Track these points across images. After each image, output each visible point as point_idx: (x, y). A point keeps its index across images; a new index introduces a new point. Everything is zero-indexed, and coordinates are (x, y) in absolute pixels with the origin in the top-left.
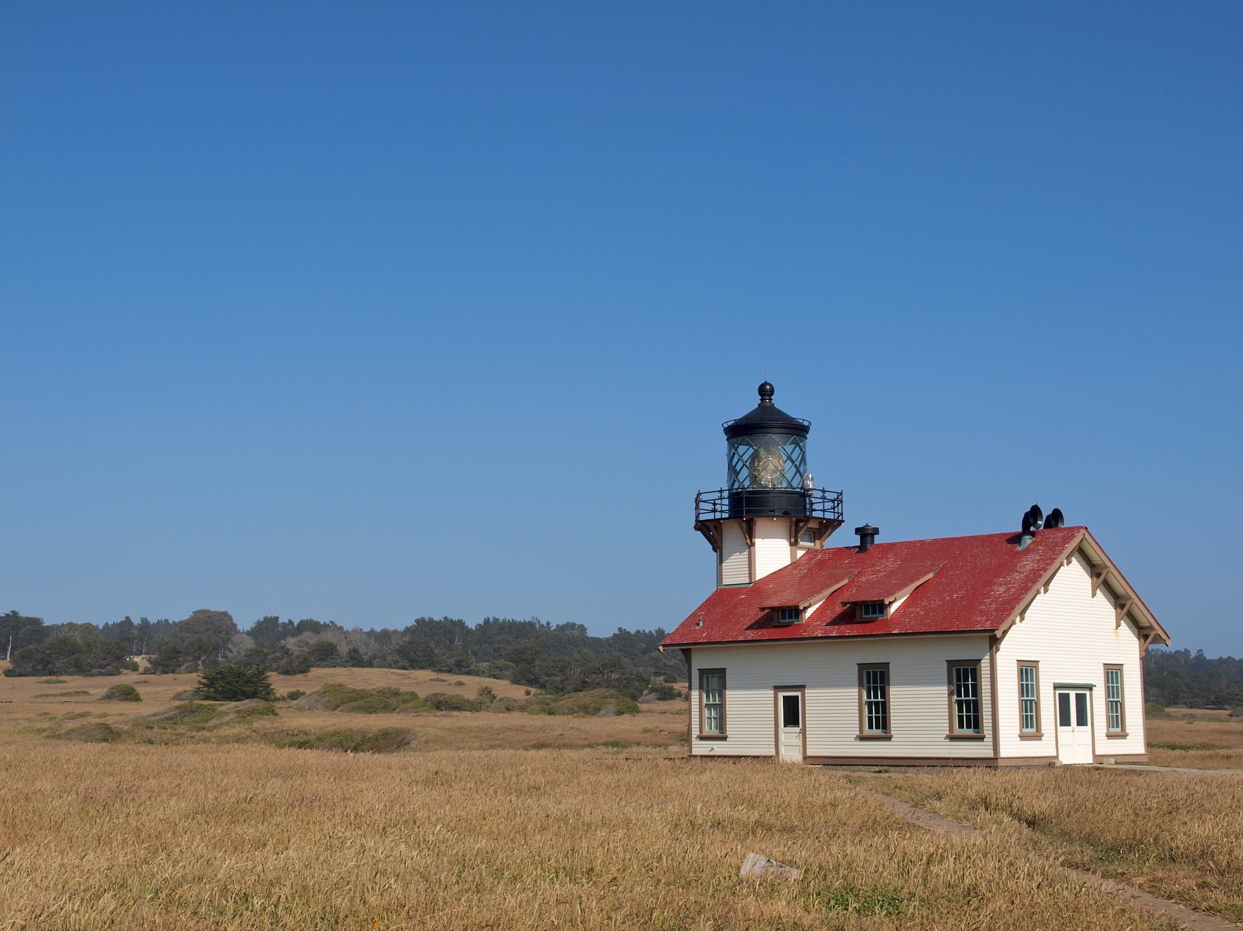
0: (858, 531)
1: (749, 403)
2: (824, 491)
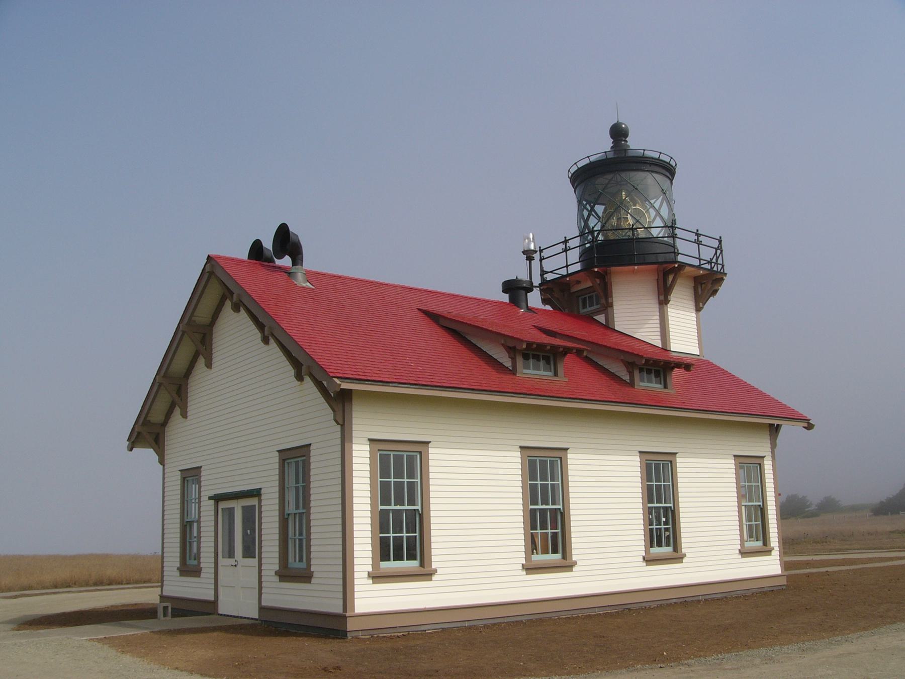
1: (603, 145)
2: (698, 234)
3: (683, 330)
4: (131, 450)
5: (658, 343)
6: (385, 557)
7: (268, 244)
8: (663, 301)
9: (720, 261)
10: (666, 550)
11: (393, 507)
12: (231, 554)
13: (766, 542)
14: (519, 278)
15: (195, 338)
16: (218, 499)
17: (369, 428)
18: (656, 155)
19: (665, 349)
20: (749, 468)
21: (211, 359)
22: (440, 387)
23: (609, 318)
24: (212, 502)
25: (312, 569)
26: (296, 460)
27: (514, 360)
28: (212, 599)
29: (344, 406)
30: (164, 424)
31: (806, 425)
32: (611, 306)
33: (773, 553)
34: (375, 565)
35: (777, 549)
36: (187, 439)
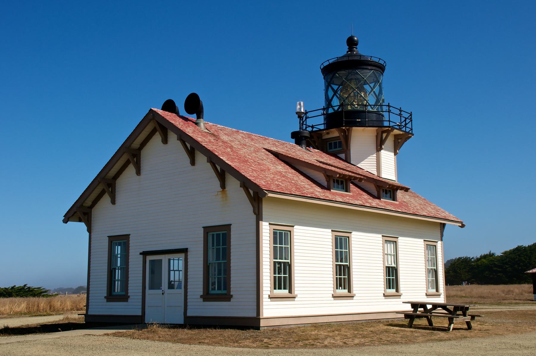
1: (342, 50)
2: (401, 111)
3: (386, 166)
4: (65, 221)
5: (375, 173)
8: (379, 148)
9: (409, 125)
10: (393, 291)
11: (284, 261)
13: (437, 290)
18: (377, 60)
20: (431, 248)
21: (140, 167)
22: (280, 192)
24: (142, 256)
25: (231, 294)
27: (328, 182)
28: (139, 313)
31: (460, 225)
33: (441, 296)
35: (443, 294)
36: (111, 217)
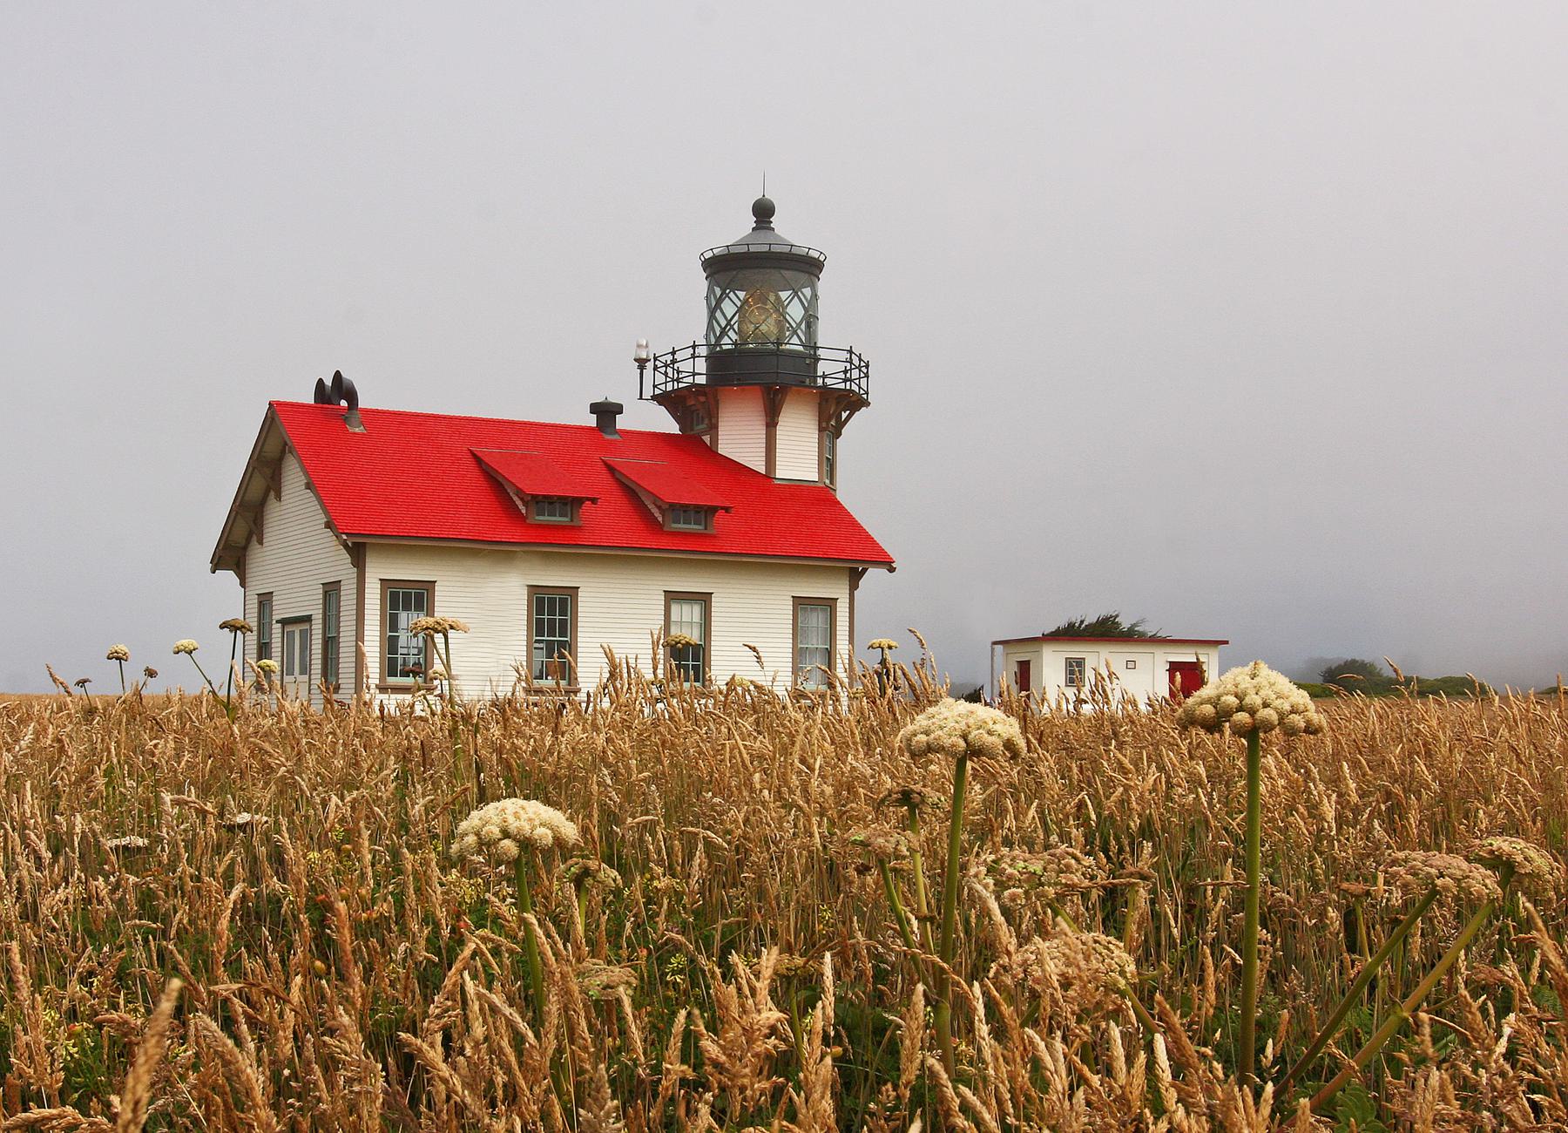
0: (595, 408)
1: (571, 336)
6: (392, 673)
7: (328, 382)
12: (291, 673)
14: (611, 400)
15: (265, 471)
16: (284, 622)
17: (378, 571)
19: (769, 477)
23: (715, 440)
26: (331, 591)
29: (771, 426)
30: (245, 548)
32: (717, 428)
34: (382, 678)
36: (268, 562)
